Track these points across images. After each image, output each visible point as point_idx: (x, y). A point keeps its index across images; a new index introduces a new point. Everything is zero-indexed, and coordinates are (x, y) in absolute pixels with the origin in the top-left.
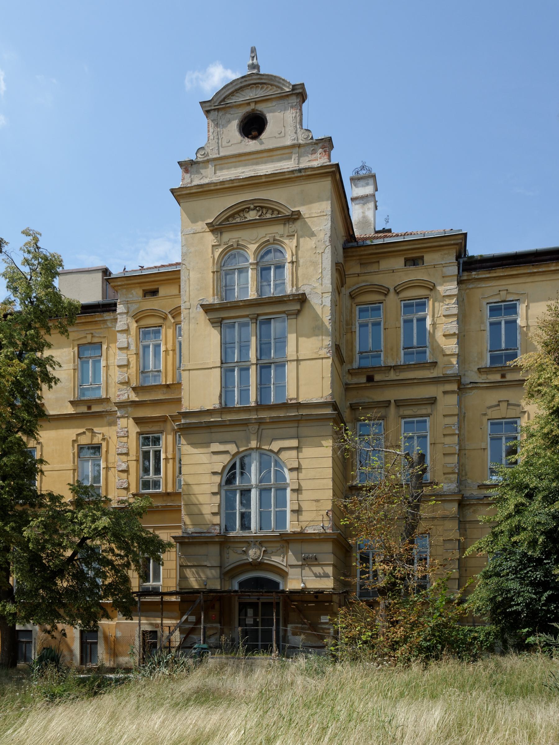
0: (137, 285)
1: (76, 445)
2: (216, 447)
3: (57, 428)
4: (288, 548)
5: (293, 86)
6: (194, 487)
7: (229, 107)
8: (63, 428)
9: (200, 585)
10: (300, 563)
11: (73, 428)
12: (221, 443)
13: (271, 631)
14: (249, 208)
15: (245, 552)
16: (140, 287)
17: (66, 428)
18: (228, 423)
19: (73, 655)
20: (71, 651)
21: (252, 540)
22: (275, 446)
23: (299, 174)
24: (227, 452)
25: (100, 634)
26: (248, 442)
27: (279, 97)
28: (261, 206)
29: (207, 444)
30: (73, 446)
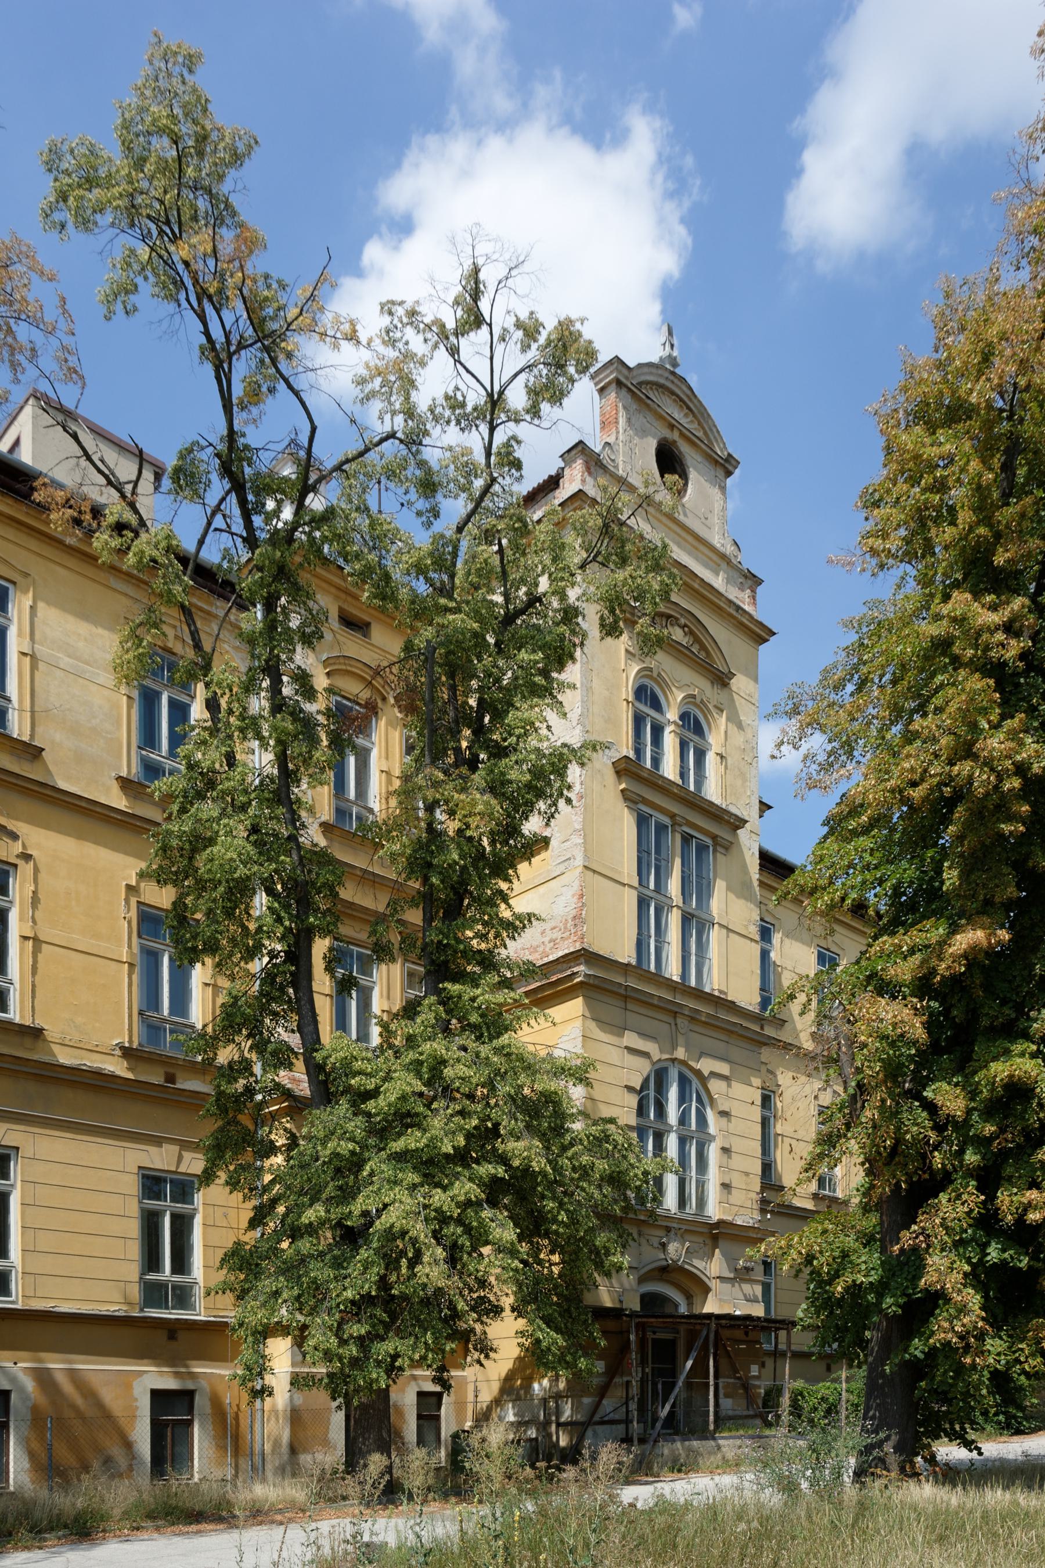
0: (333, 590)
1: (133, 901)
2: (631, 1039)
3: (80, 836)
4: (715, 1246)
5: (729, 455)
6: (601, 1106)
7: (648, 405)
8: (96, 842)
9: (613, 1301)
10: (732, 1275)
11: (126, 853)
12: (642, 1034)
13: (707, 1385)
14: (677, 619)
15: (664, 1246)
16: (337, 598)
17: (106, 846)
18: (656, 1002)
19: (134, 1458)
20: (128, 1445)
21: (675, 1225)
22: (706, 1065)
23: (734, 613)
24: (646, 1055)
25: (200, 1402)
26: (674, 1048)
27: (710, 456)
28: (694, 629)
29: (619, 1029)
30: (127, 901)
